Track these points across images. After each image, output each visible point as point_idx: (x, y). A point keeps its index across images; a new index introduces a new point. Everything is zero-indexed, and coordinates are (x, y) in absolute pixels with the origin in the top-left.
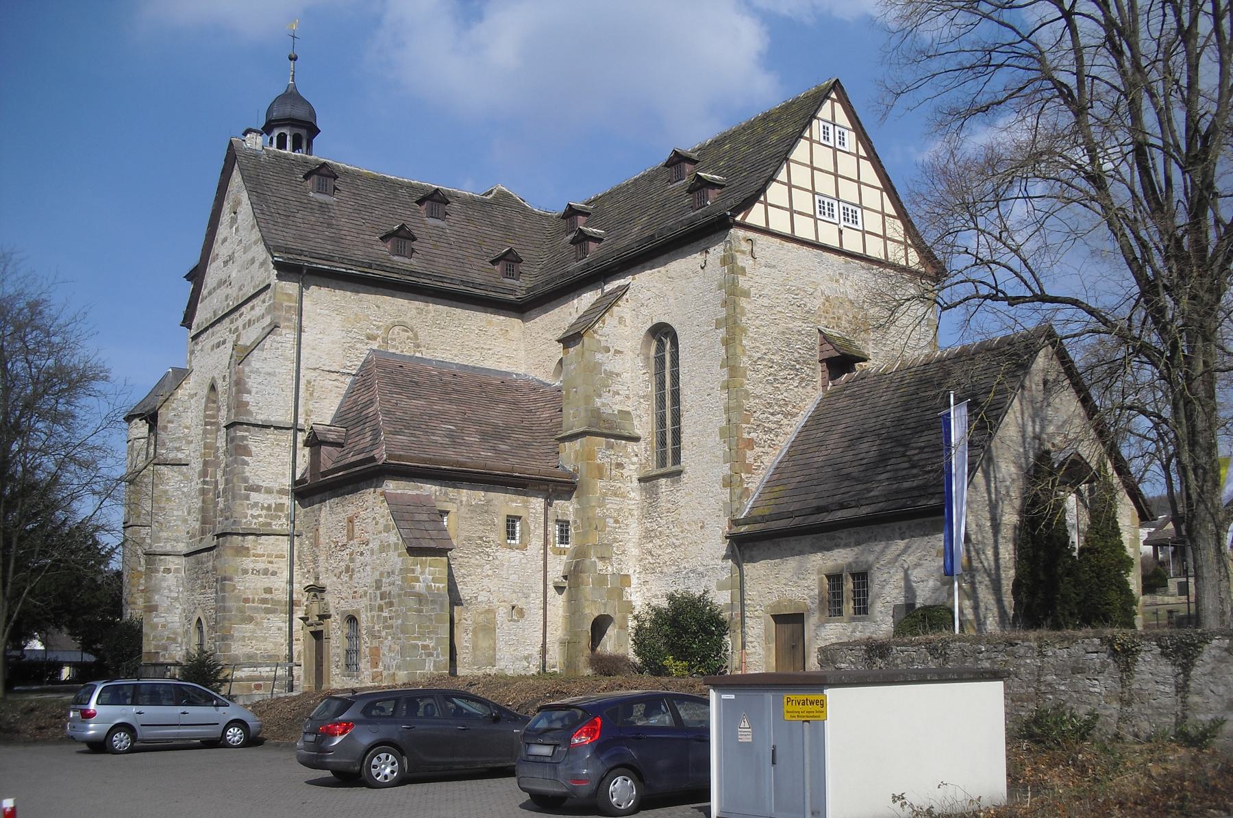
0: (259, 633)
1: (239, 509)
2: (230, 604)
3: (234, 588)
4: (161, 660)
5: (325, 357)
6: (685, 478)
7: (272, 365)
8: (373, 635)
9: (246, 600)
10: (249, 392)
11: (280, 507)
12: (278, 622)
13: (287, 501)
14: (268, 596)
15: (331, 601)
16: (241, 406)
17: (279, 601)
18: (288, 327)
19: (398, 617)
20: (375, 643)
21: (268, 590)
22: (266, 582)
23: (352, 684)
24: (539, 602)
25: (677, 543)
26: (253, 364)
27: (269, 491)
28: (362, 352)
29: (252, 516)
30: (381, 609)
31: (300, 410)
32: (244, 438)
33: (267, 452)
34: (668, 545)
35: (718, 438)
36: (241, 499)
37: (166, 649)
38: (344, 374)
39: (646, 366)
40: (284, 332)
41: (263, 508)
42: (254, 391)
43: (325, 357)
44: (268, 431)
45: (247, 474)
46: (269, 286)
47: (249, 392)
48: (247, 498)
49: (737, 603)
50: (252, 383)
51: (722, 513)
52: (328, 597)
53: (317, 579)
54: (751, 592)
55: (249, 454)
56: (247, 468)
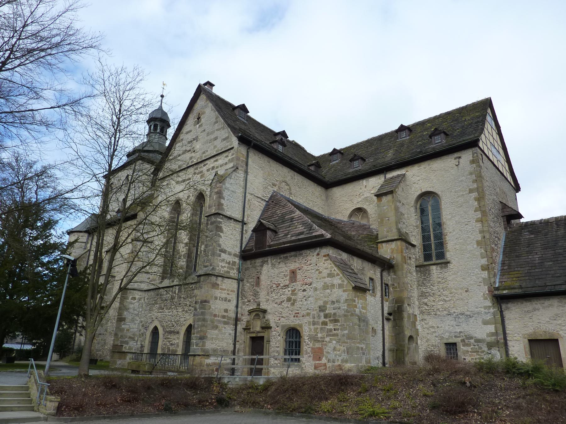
0: (220, 336)
1: (216, 261)
2: (208, 317)
3: (210, 308)
4: (124, 350)
5: (256, 189)
6: (450, 266)
7: (234, 187)
8: (314, 339)
9: (215, 316)
10: (224, 199)
11: (234, 263)
12: (229, 330)
13: (237, 260)
14: (226, 314)
15: (272, 319)
16: (220, 205)
17: (231, 318)
18: (241, 170)
19: (343, 329)
20: (318, 345)
21: (226, 311)
22: (225, 305)
23: (293, 371)
24: (381, 326)
25: (447, 299)
26: (226, 184)
27: (230, 254)
28: (271, 190)
29: (221, 266)
30: (325, 323)
31: (246, 214)
32: (220, 222)
33: (230, 232)
34: (439, 301)
35: (475, 246)
36: (217, 256)
37: (127, 343)
38: (263, 200)
39: (416, 212)
40: (240, 172)
41: (226, 263)
42: (226, 198)
43: (256, 189)
44: (229, 221)
45: (221, 243)
46: (233, 148)
47: (224, 199)
48: (220, 256)
49: (500, 331)
50: (226, 194)
51: (482, 284)
52: (268, 316)
53: (259, 305)
54: (510, 327)
55: (222, 232)
56: (221, 240)
